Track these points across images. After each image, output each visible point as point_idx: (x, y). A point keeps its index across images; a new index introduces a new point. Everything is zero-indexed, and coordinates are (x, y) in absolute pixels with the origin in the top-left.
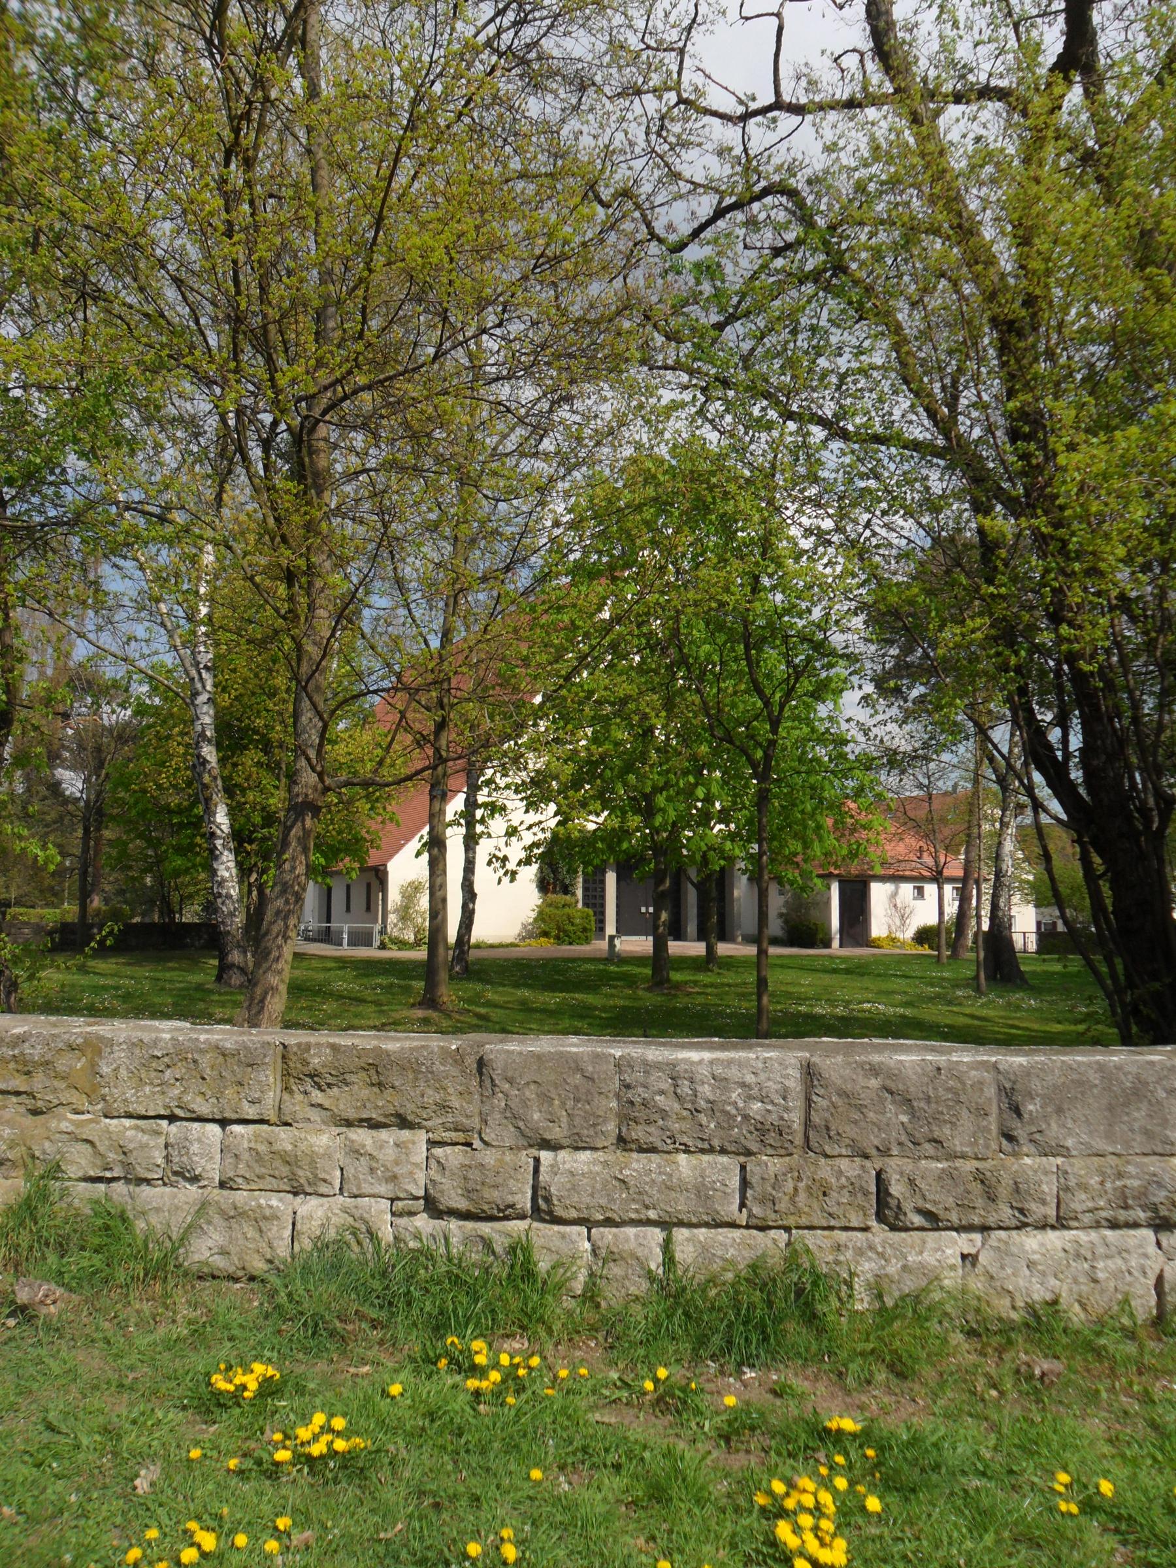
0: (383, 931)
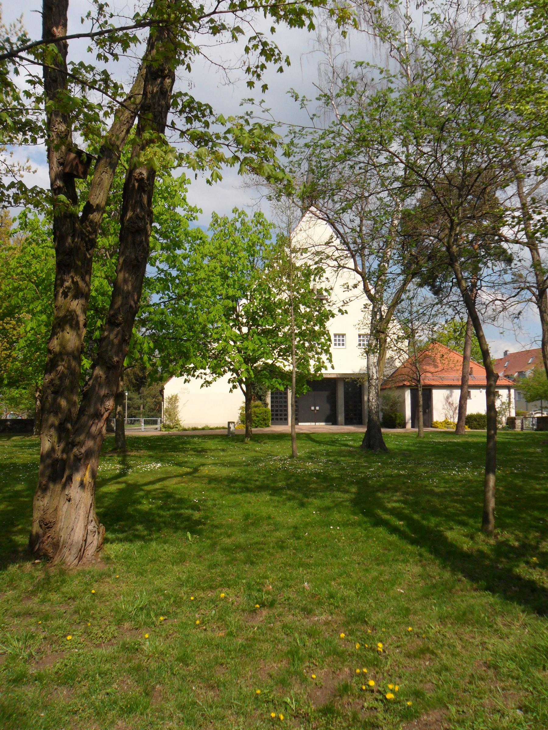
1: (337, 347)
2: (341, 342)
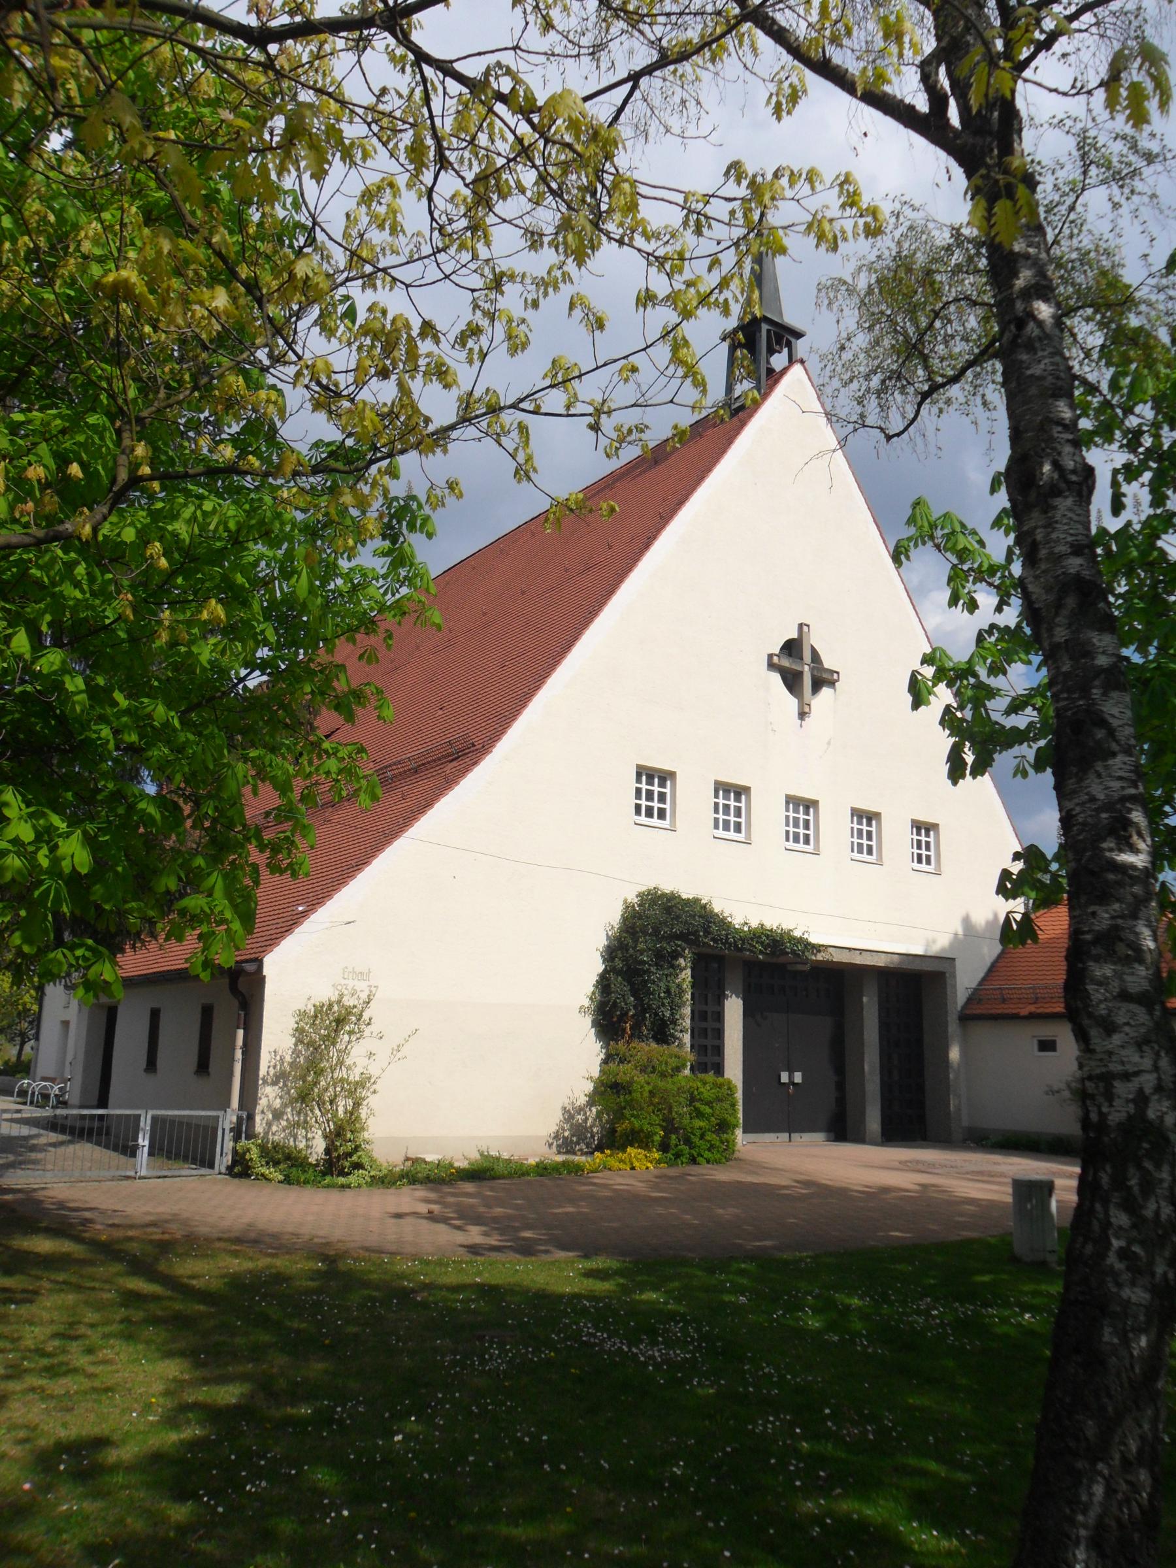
0: (243, 1129)
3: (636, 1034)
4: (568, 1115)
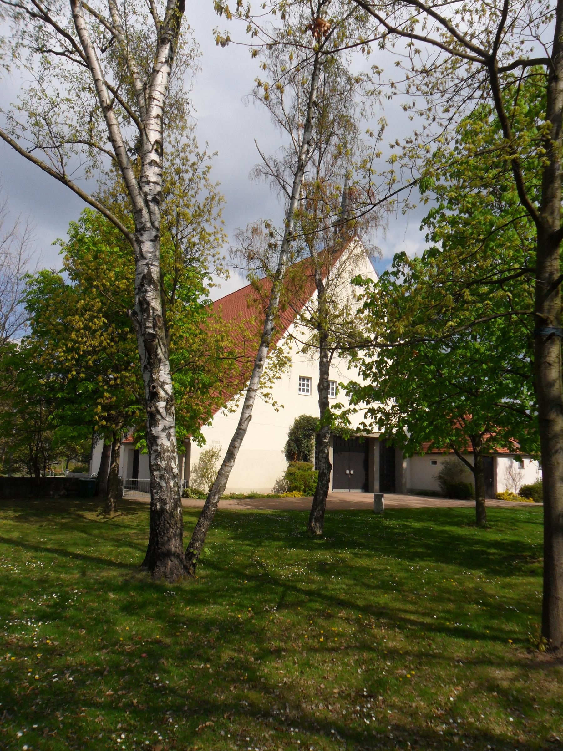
0: (186, 485)
1: (301, 393)
2: (306, 388)
3: (298, 459)
4: (278, 482)
